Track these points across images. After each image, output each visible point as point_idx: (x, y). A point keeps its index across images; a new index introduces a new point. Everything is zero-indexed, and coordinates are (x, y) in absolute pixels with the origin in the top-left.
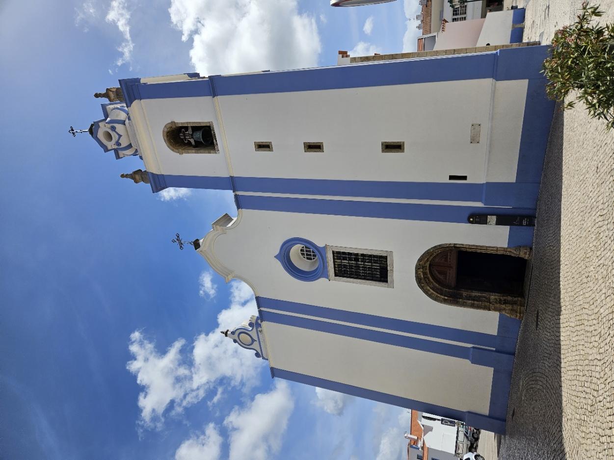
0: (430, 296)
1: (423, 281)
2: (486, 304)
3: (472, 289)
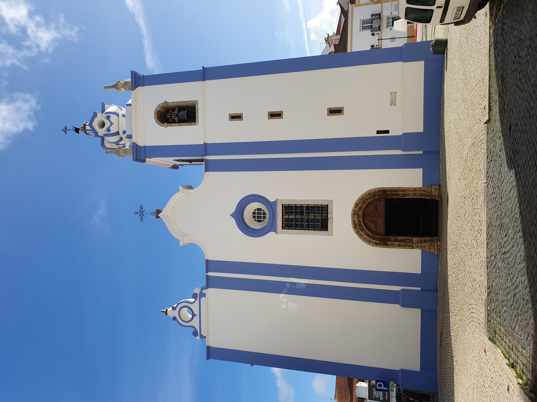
0: (364, 239)
1: (358, 227)
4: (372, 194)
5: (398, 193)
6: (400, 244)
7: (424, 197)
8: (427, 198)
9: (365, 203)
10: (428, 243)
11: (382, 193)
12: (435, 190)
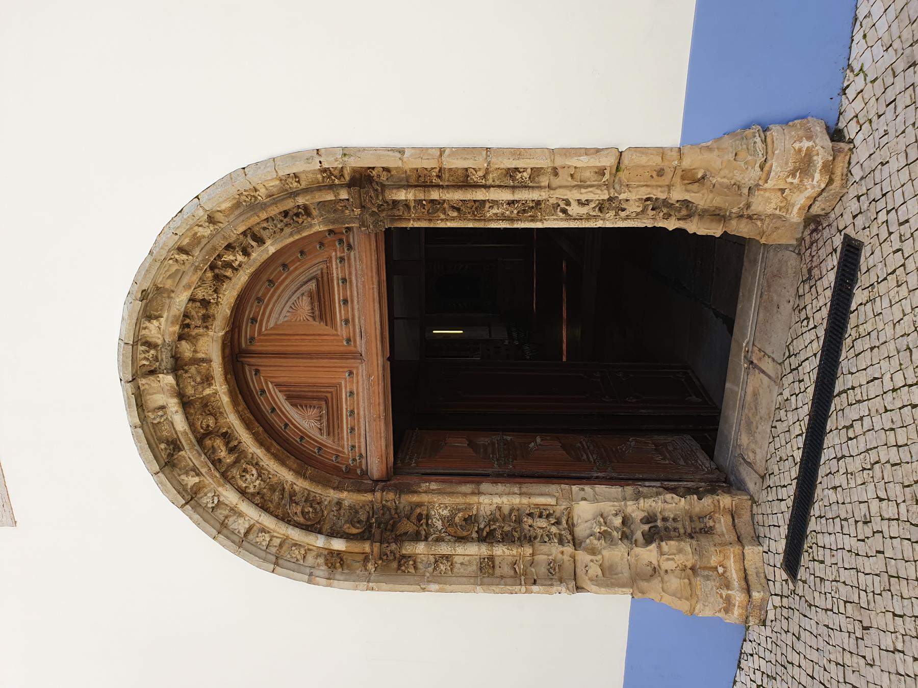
1: (190, 455)
2: (554, 550)
3: (477, 477)
4: (264, 207)
5: (480, 195)
6: (491, 558)
7: (671, 225)
8: (694, 227)
9: (229, 273)
10: (680, 551)
11: (344, 195)
12: (793, 174)
